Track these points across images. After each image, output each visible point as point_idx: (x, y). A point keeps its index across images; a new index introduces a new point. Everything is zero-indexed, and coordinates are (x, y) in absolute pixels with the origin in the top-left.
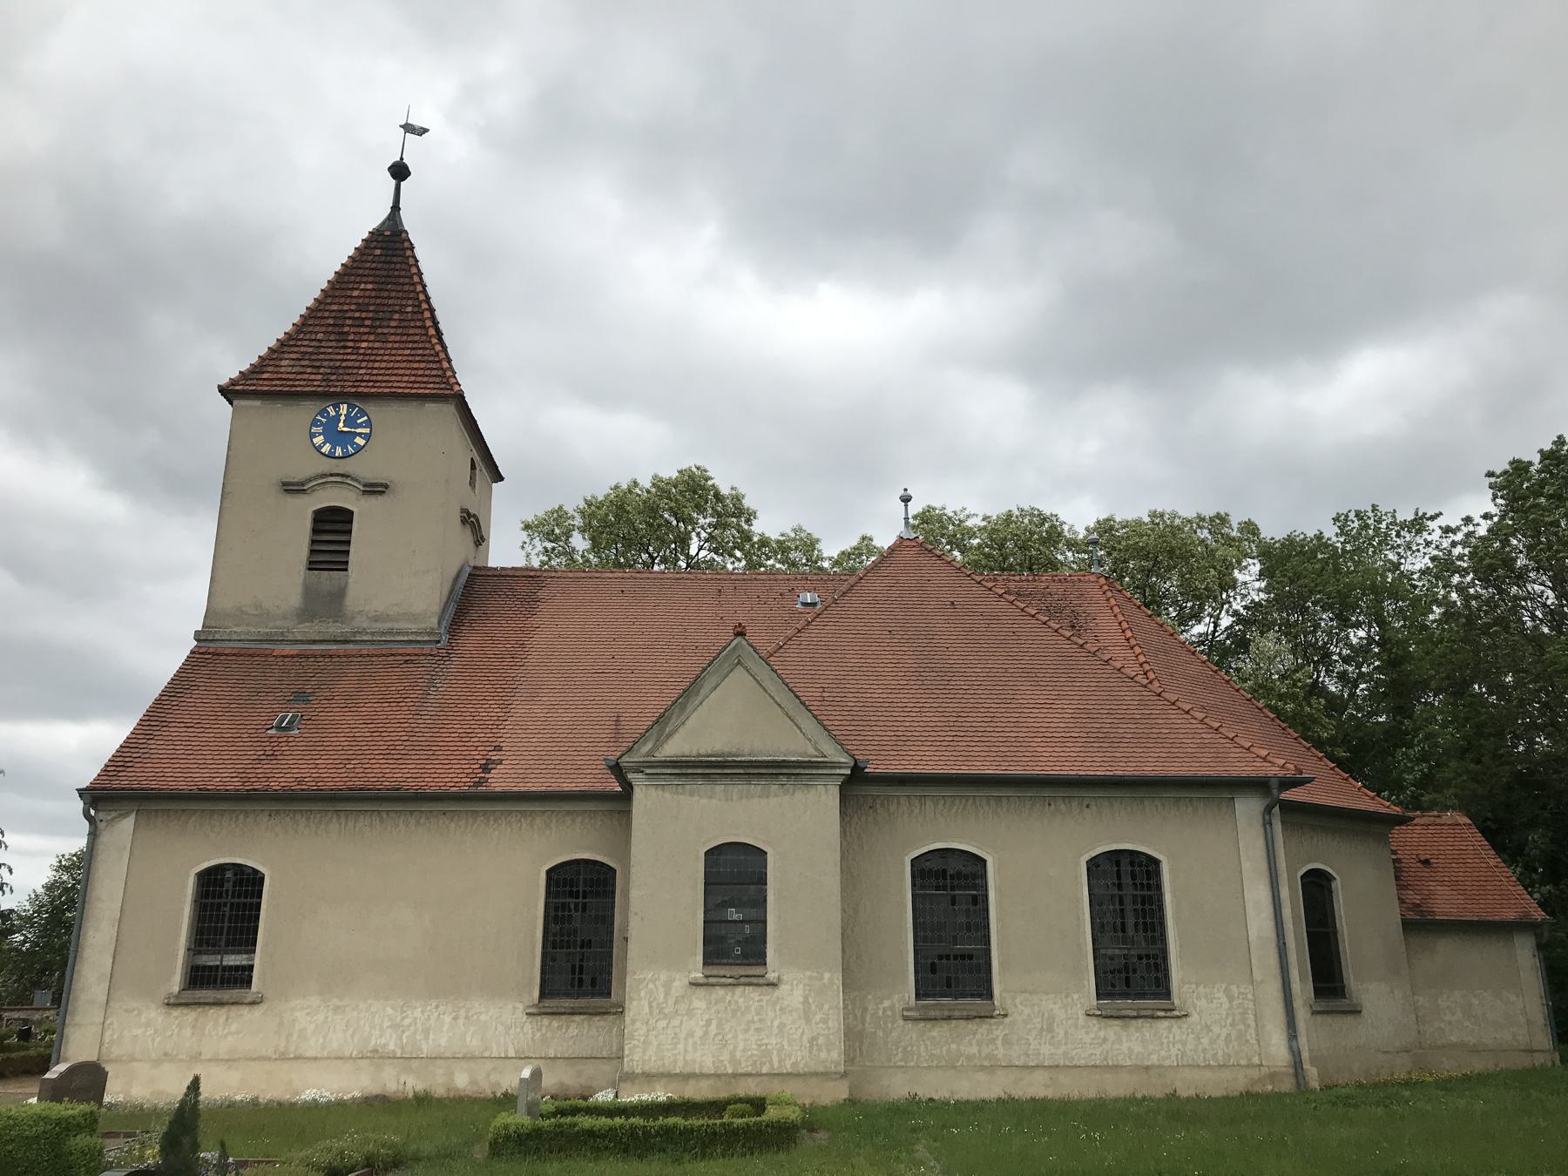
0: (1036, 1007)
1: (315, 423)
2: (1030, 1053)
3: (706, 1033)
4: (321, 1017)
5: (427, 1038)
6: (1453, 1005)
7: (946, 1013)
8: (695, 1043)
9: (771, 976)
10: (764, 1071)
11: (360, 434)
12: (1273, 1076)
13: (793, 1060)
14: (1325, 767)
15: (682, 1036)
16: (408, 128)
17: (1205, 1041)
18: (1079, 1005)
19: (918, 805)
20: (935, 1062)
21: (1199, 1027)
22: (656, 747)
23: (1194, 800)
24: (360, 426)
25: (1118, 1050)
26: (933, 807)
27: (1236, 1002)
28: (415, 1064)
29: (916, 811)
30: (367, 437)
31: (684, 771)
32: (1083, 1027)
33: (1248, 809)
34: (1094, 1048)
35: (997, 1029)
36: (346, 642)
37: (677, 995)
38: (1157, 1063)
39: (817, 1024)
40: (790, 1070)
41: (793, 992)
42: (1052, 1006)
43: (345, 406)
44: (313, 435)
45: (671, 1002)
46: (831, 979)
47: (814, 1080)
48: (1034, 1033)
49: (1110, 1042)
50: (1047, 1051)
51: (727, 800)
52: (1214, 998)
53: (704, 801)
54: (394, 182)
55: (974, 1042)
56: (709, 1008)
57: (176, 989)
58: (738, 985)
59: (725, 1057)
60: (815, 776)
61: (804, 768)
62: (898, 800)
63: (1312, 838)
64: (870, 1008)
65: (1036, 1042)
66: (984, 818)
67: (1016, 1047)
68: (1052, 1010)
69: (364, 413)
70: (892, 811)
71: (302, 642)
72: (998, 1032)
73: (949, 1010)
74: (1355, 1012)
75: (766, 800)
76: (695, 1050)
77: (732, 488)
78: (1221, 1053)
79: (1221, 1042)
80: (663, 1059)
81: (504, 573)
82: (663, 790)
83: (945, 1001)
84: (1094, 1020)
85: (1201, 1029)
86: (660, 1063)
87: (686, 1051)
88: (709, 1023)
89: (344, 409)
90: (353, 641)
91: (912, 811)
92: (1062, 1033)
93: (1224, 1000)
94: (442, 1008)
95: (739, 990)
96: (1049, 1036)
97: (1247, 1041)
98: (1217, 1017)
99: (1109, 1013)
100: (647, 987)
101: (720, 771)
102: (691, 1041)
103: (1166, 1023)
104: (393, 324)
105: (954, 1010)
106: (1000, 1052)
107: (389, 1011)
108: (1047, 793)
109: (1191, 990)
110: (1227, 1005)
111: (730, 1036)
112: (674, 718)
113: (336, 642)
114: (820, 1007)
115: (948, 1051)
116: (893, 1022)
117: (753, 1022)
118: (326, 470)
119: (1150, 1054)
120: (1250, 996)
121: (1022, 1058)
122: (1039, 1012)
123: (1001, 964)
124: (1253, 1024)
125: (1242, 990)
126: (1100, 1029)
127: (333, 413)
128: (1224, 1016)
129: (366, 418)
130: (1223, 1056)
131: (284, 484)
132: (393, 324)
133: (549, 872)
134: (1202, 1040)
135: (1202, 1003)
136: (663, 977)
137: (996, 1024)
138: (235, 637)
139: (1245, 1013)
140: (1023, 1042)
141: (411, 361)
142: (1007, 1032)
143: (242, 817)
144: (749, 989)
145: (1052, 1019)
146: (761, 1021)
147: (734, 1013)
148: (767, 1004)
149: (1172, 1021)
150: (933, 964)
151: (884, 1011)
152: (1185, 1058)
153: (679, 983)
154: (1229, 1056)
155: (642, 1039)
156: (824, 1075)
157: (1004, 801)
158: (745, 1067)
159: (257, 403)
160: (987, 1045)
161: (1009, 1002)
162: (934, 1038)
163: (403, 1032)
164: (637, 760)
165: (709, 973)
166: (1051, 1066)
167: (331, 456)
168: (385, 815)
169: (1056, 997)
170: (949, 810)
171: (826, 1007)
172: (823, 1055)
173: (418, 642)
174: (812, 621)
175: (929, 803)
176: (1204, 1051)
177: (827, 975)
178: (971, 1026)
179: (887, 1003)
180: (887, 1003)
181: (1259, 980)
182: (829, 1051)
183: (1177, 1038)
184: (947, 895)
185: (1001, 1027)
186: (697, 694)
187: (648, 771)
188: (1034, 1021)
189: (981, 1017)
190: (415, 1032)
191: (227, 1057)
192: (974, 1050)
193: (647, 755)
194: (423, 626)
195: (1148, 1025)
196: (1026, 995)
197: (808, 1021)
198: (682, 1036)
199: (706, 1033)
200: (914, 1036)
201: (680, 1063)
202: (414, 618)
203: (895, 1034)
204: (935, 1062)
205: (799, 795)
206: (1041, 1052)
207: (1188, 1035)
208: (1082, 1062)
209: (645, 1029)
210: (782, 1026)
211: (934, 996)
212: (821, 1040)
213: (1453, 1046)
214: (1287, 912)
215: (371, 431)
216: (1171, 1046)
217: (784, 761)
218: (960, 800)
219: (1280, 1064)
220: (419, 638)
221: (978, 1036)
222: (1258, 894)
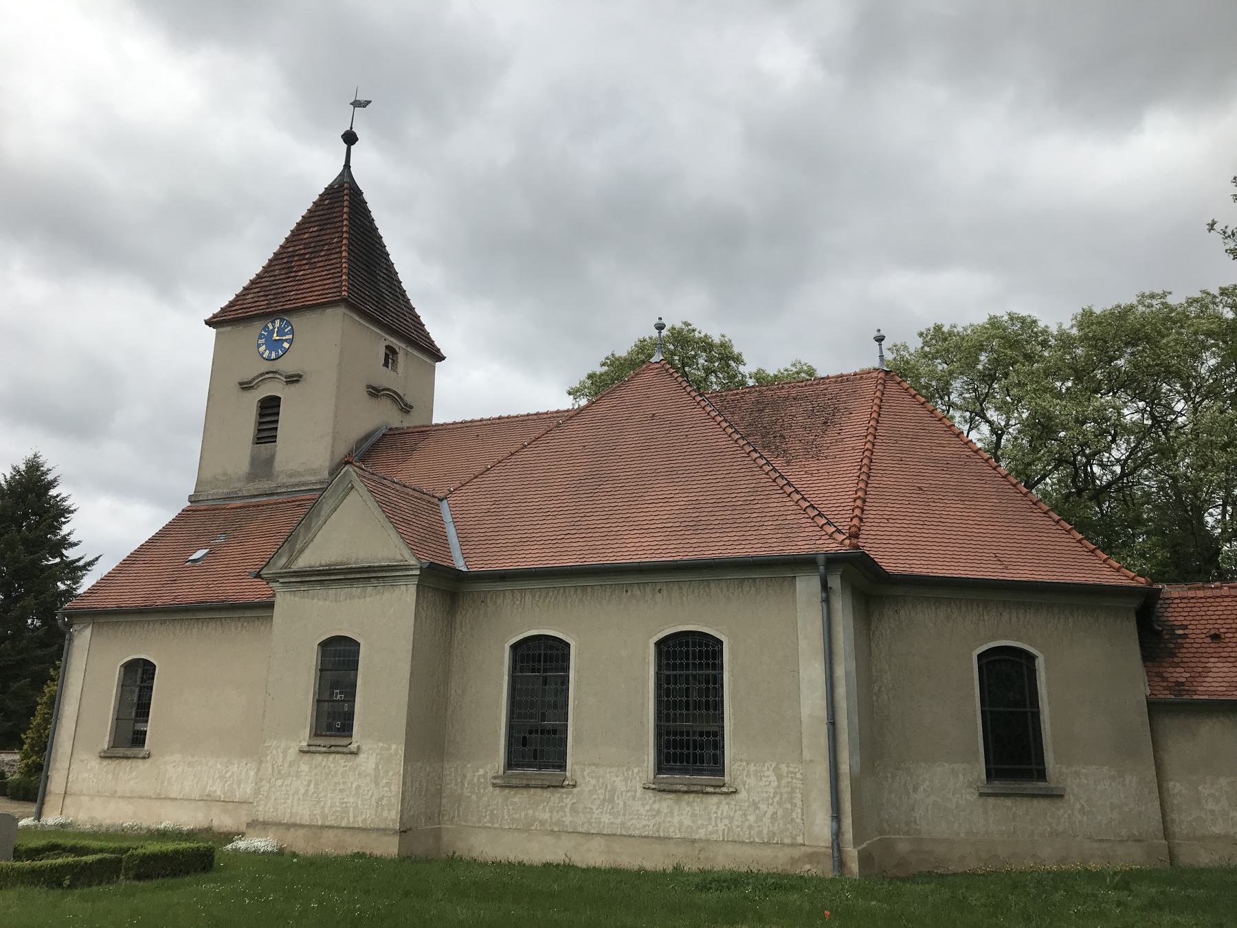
0: (601, 779)
1: (260, 338)
2: (592, 821)
3: (307, 791)
4: (180, 769)
5: (239, 787)
6: (1217, 794)
7: (525, 782)
8: (299, 799)
9: (353, 747)
10: (343, 825)
11: (286, 340)
12: (812, 857)
13: (364, 817)
14: (1072, 541)
15: (291, 792)
16: (357, 104)
17: (752, 818)
18: (638, 778)
19: (519, 597)
20: (515, 825)
21: (747, 803)
22: (291, 561)
23: (758, 581)
24: (287, 334)
25: (669, 822)
26: (531, 599)
27: (784, 781)
28: (230, 806)
29: (518, 602)
30: (291, 342)
31: (304, 579)
32: (640, 799)
33: (807, 586)
34: (648, 820)
35: (567, 798)
36: (272, 494)
37: (291, 759)
38: (704, 838)
39: (383, 787)
40: (361, 825)
41: (367, 761)
42: (615, 779)
44: (259, 346)
45: (286, 765)
46: (396, 750)
47: (374, 835)
48: (597, 802)
49: (663, 815)
50: (606, 820)
51: (336, 601)
52: (764, 776)
53: (321, 603)
54: (345, 146)
56: (310, 771)
57: (106, 747)
58: (330, 753)
59: (318, 811)
60: (397, 578)
61: (386, 571)
62: (504, 594)
65: (598, 811)
66: (572, 606)
67: (581, 815)
68: (614, 782)
69: (289, 323)
70: (498, 603)
71: (247, 497)
73: (528, 779)
74: (1055, 796)
75: (363, 600)
76: (299, 805)
78: (765, 831)
79: (766, 820)
80: (277, 811)
81: (410, 430)
82: (295, 596)
83: (531, 771)
84: (650, 793)
85: (749, 807)
86: (275, 814)
87: (292, 806)
88: (310, 782)
89: (277, 323)
90: (276, 493)
91: (514, 603)
92: (621, 804)
93: (773, 778)
94: (249, 765)
95: (331, 757)
96: (610, 807)
97: (792, 820)
98: (765, 795)
99: (663, 787)
100: (271, 753)
101: (328, 578)
102: (296, 797)
103: (715, 799)
104: (323, 253)
105: (531, 780)
106: (568, 819)
107: (219, 766)
108: (558, 584)
109: (742, 768)
110: (775, 784)
111: (322, 794)
112: (301, 538)
114: (387, 772)
115: (526, 815)
116: (485, 788)
117: (339, 783)
119: (699, 828)
120: (798, 776)
121: (586, 825)
123: (575, 739)
124: (799, 804)
125: (791, 769)
126: (654, 802)
127: (271, 328)
128: (771, 796)
130: (768, 834)
131: (241, 384)
132: (323, 253)
133: (659, 644)
134: (749, 817)
135: (752, 781)
136: (283, 745)
137: (566, 793)
138: (210, 497)
139: (793, 791)
140: (588, 810)
142: (575, 801)
143: (146, 625)
144: (338, 756)
145: (613, 790)
146: (344, 783)
147: (327, 775)
148: (350, 769)
149: (722, 797)
150: (524, 738)
151: (479, 779)
152: (731, 834)
153: (293, 751)
154: (774, 834)
155: (265, 794)
156: (384, 831)
157: (589, 590)
158: (331, 821)
159: (229, 328)
161: (579, 774)
163: (226, 782)
164: (274, 572)
165: (312, 743)
166: (608, 835)
167: (269, 359)
168: (224, 621)
169: (618, 771)
170: (544, 601)
171: (391, 773)
172: (385, 814)
173: (315, 490)
174: (529, 444)
175: (528, 595)
176: (750, 827)
177: (394, 747)
178: (546, 794)
179: (481, 772)
180: (481, 772)
181: (808, 759)
182: (389, 810)
183: (725, 813)
184: (540, 676)
185: (570, 796)
186: (319, 515)
187: (281, 580)
188: (598, 792)
189: (554, 787)
190: (232, 783)
191: (129, 795)
192: (547, 816)
193: (284, 567)
194: (319, 477)
195: (699, 800)
196: (593, 767)
197: (377, 784)
198: (291, 792)
199: (307, 791)
200: (500, 800)
201: (288, 815)
202: (314, 472)
203: (485, 799)
204: (515, 825)
205: (387, 595)
206: (602, 820)
207: (736, 811)
208: (637, 833)
209: (268, 786)
210: (358, 787)
211: (522, 766)
212: (384, 802)
213: (1217, 838)
214: (841, 691)
216: (719, 821)
217: (369, 567)
218: (553, 591)
219: (822, 844)
220: (314, 487)
221: (551, 804)
222: (812, 672)
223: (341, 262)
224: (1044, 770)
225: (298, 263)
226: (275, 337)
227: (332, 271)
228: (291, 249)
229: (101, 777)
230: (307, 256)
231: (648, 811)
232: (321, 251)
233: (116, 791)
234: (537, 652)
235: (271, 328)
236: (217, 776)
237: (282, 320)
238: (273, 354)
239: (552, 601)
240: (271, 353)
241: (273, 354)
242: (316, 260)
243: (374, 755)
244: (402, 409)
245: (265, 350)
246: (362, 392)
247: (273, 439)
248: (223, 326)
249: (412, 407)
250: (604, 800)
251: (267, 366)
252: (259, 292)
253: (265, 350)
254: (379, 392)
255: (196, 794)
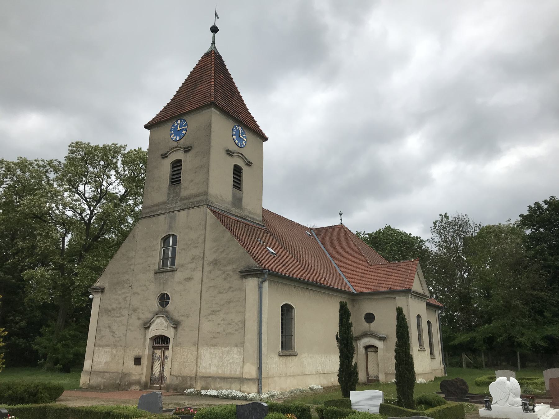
1: (171, 131)
24: (184, 126)
30: (186, 130)
36: (244, 219)
44: (171, 135)
77: (213, 132)
113: (243, 218)
167: (176, 141)
215: (187, 127)
223: (211, 73)
226: (179, 129)
229: (280, 366)
233: (287, 373)
235: (176, 125)
236: (319, 363)
237: (181, 119)
238: (178, 137)
240: (177, 137)
241: (178, 137)
245: (174, 137)
246: (224, 153)
249: (252, 163)
251: (175, 144)
253: (174, 137)
254: (233, 154)
255: (314, 372)
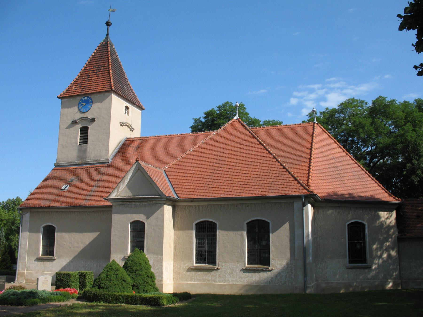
43: (86, 97)
55: (210, 276)
63: (355, 211)
64: (182, 266)
72: (217, 274)
78: (283, 281)
104: (101, 70)
109: (275, 262)
118: (82, 117)
120: (294, 264)
122: (229, 268)
125: (292, 262)
129: (91, 100)
132: (101, 70)
133: (248, 224)
141: (103, 81)
143: (50, 213)
145: (233, 270)
160: (214, 277)
162: (199, 275)
176: (278, 280)
224: (366, 260)
225: (91, 74)
227: (106, 78)
228: (88, 68)
230: (95, 71)
231: (244, 276)
232: (101, 69)
234: (204, 226)
239: (210, 209)
242: (99, 73)
243: (152, 260)
244: (131, 130)
247: (86, 143)
248: (64, 99)
249: (134, 129)
250: (230, 273)
252: (77, 85)
